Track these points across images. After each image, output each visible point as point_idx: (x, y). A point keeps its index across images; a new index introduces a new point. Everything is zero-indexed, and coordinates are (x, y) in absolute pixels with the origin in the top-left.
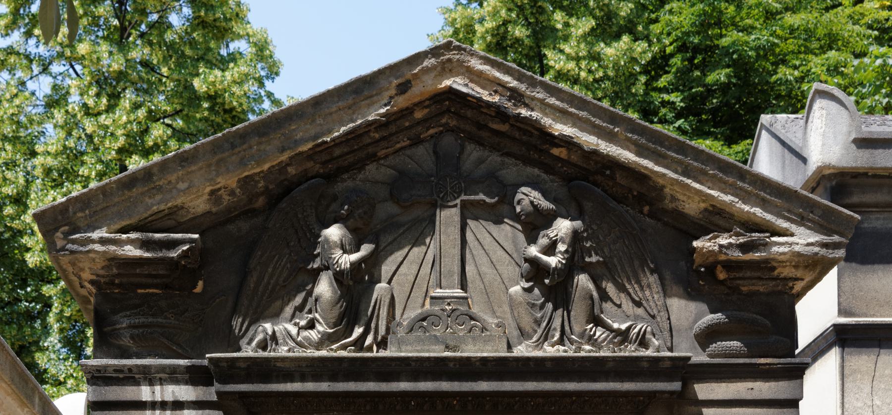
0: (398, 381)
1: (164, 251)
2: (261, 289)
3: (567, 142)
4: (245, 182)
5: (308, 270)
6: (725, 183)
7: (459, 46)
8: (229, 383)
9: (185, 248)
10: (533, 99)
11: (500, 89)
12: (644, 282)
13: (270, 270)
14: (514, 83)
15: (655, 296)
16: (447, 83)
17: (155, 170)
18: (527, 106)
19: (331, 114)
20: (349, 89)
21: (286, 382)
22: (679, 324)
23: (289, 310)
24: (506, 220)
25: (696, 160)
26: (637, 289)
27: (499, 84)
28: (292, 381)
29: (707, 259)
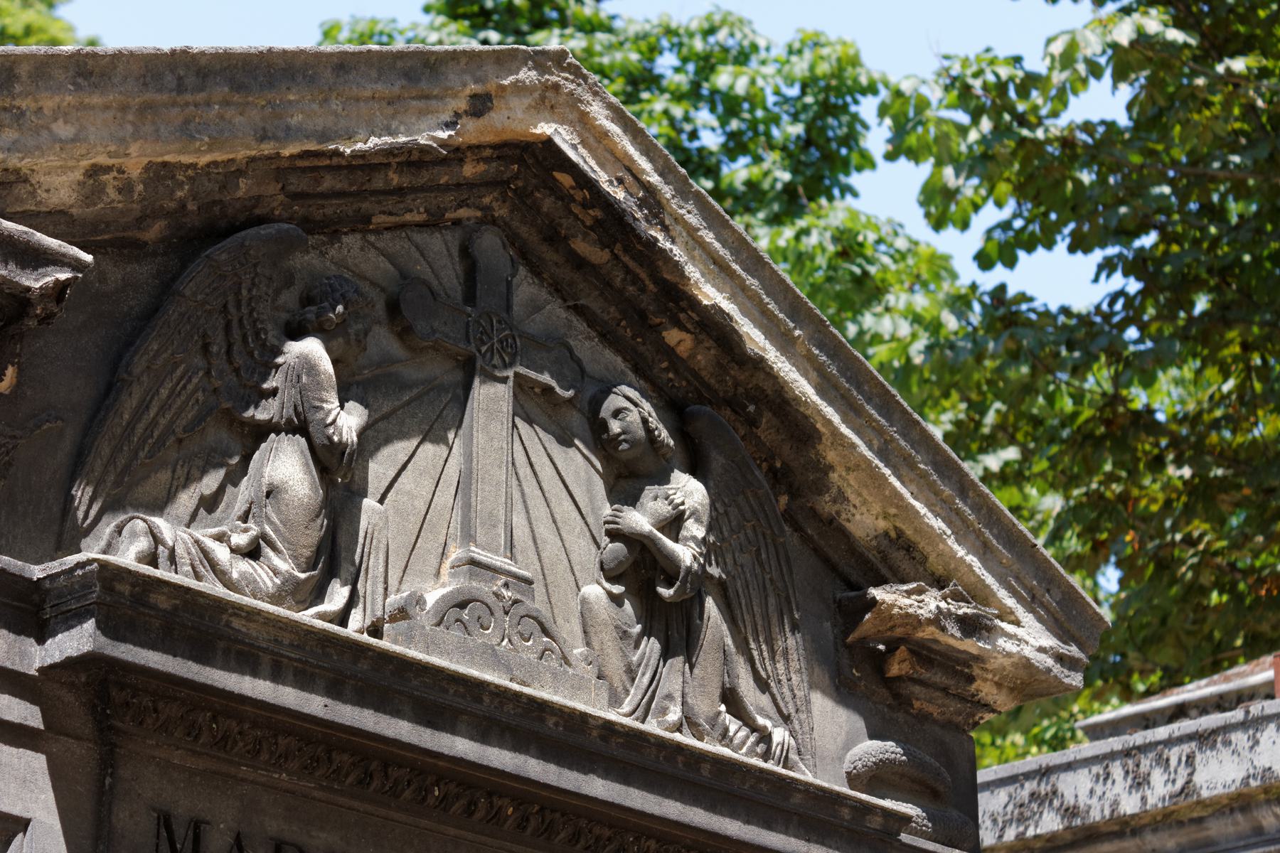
0: (454, 732)
1: (12, 266)
2: (140, 428)
3: (714, 328)
4: (160, 173)
5: (243, 423)
6: (937, 493)
7: (578, 68)
8: (124, 640)
9: (63, 276)
10: (679, 220)
11: (629, 179)
12: (780, 644)
13: (164, 392)
14: (654, 179)
15: (794, 677)
16: (545, 128)
17: (23, 70)
18: (665, 229)
19: (358, 100)
20: (399, 64)
21: (243, 673)
22: (830, 744)
23: (186, 500)
24: (577, 442)
25: (904, 436)
26: (765, 654)
27: (629, 170)
28: (255, 674)
29: (892, 628)
